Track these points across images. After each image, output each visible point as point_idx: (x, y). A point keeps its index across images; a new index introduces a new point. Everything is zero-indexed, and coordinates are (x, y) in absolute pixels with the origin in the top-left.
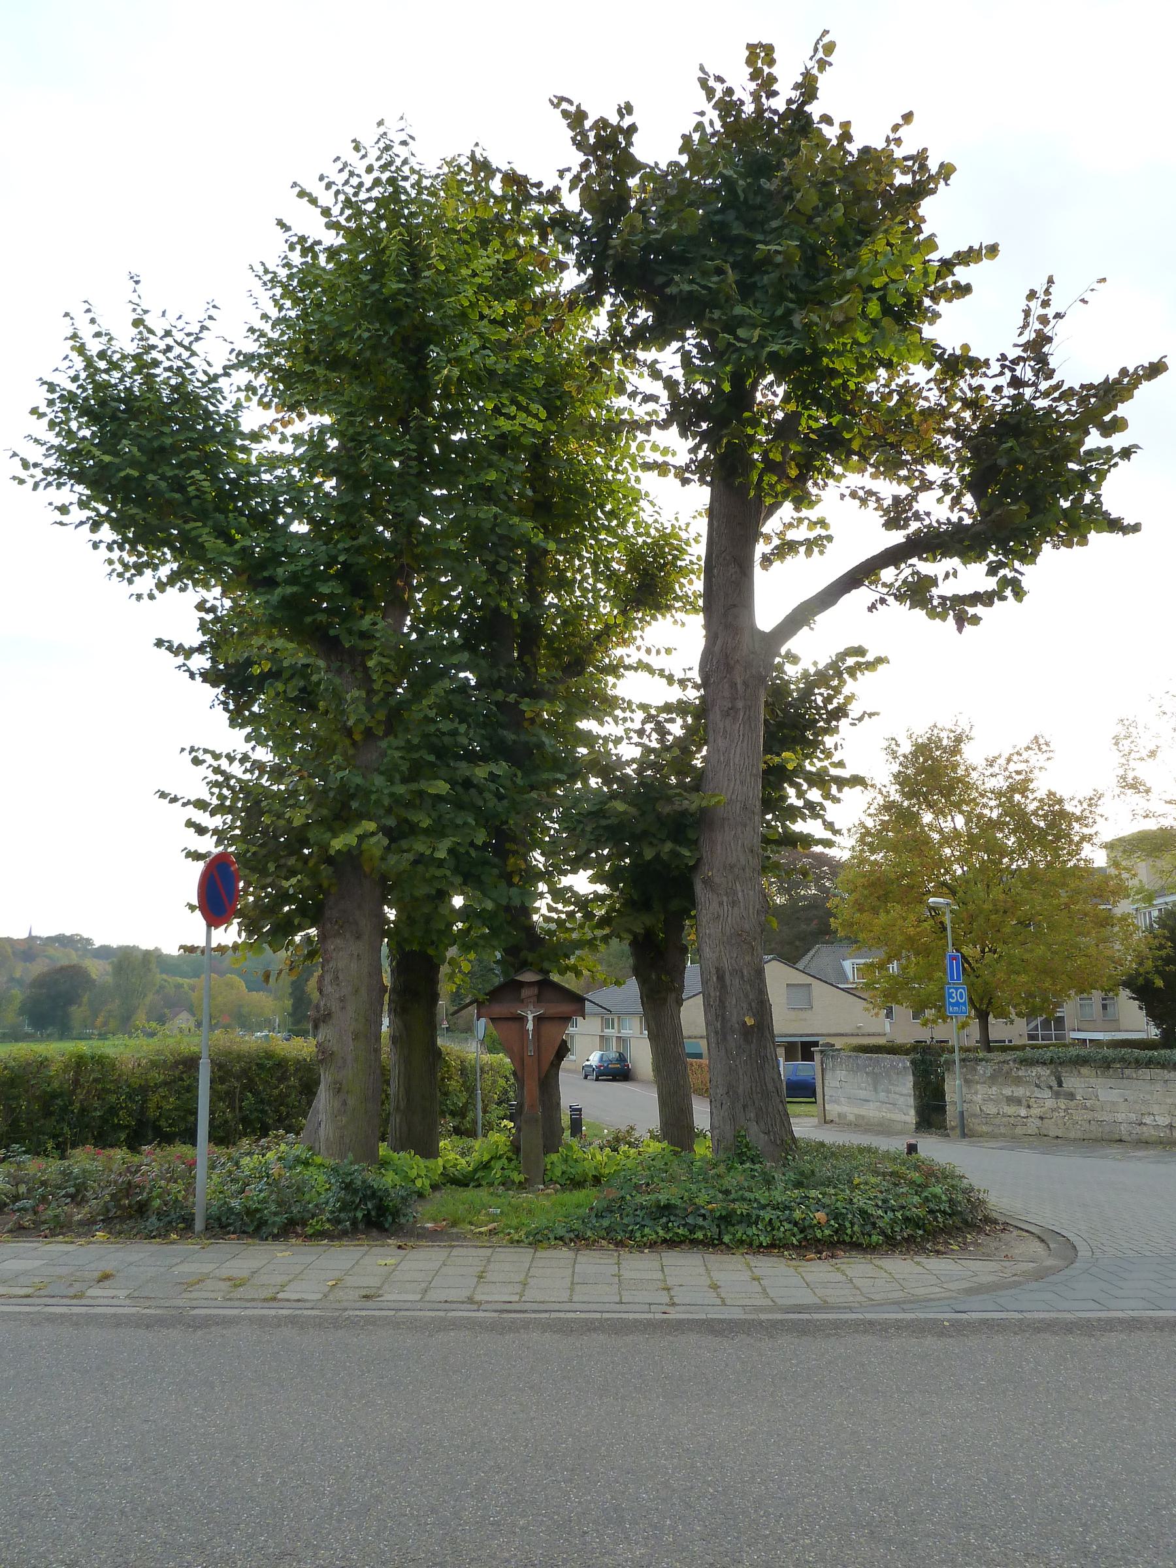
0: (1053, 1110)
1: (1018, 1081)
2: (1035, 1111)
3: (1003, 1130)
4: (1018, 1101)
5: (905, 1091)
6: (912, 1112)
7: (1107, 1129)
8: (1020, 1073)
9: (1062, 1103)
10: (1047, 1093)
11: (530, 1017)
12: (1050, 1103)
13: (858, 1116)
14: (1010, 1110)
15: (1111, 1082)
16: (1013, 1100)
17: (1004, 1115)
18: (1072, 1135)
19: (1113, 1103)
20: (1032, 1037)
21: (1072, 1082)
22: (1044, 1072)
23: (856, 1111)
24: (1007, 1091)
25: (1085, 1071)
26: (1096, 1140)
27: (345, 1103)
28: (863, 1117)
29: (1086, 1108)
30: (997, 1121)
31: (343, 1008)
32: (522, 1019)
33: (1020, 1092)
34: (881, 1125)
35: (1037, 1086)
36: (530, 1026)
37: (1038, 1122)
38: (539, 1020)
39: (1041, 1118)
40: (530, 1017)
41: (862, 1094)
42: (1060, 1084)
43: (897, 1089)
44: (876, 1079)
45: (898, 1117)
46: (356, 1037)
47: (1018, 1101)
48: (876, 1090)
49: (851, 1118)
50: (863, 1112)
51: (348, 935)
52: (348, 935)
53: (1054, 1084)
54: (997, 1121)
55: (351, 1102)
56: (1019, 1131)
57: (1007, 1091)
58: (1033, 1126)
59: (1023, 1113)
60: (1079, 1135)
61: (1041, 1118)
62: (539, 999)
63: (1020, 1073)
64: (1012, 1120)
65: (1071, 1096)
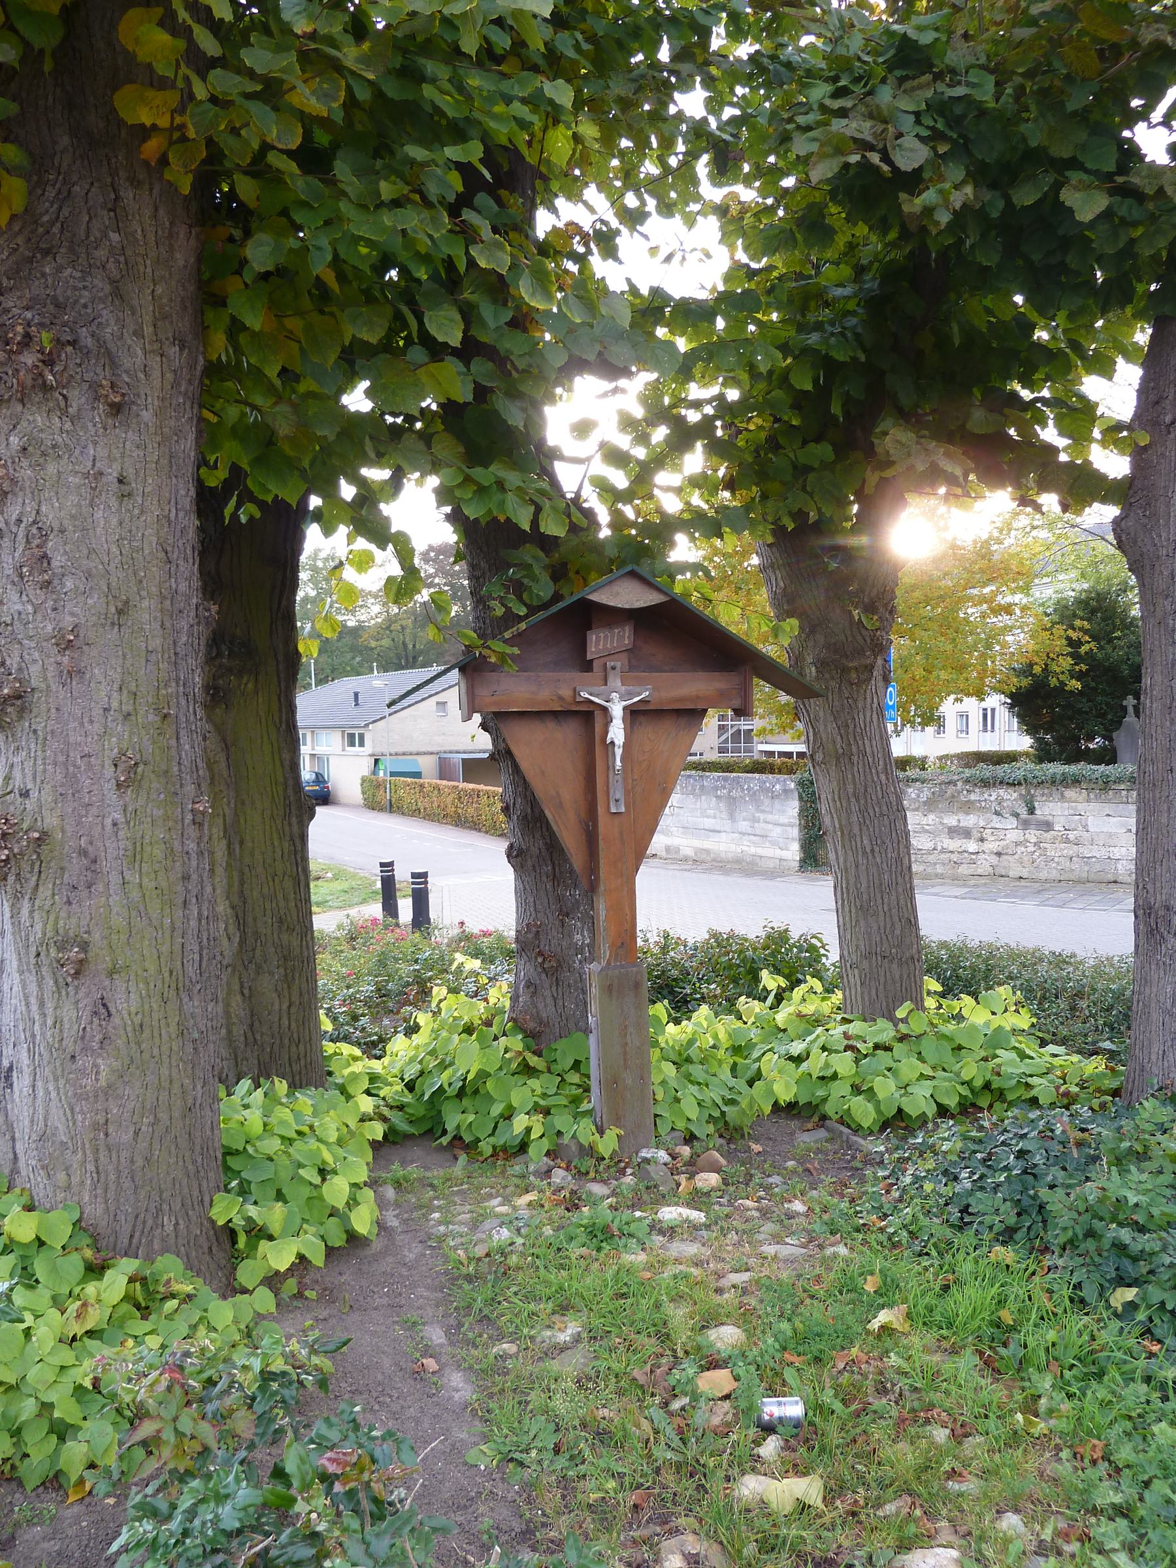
0: (1017, 844)
1: (968, 807)
2: (991, 846)
3: (939, 869)
4: (966, 833)
5: (784, 820)
6: (796, 846)
7: (1098, 867)
8: (973, 797)
9: (1032, 835)
10: (1012, 822)
11: (617, 710)
12: (1014, 835)
13: (698, 851)
14: (954, 844)
15: (1108, 808)
16: (953, 832)
17: (944, 851)
18: (1043, 875)
19: (1110, 835)
20: (722, 750)
21: (1047, 808)
22: (1010, 796)
23: (698, 843)
24: (951, 820)
25: (1070, 793)
26: (1079, 881)
27: (103, 1008)
28: (708, 851)
29: (1067, 841)
30: (931, 858)
31: (74, 673)
32: (589, 718)
33: (969, 820)
34: (738, 861)
35: (997, 813)
36: (617, 733)
37: (994, 860)
38: (634, 714)
39: (999, 854)
40: (617, 710)
41: (709, 823)
42: (1032, 811)
43: (770, 817)
44: (732, 803)
45: (786, 854)
46: (130, 778)
47: (966, 833)
48: (732, 818)
49: (689, 852)
50: (707, 844)
51: (78, 398)
52: (78, 398)
53: (1023, 812)
54: (931, 858)
55: (127, 1002)
56: (964, 870)
57: (951, 820)
58: (985, 864)
59: (972, 846)
60: (1054, 874)
61: (999, 854)
62: (636, 663)
63: (973, 797)
64: (955, 857)
65: (1047, 826)
